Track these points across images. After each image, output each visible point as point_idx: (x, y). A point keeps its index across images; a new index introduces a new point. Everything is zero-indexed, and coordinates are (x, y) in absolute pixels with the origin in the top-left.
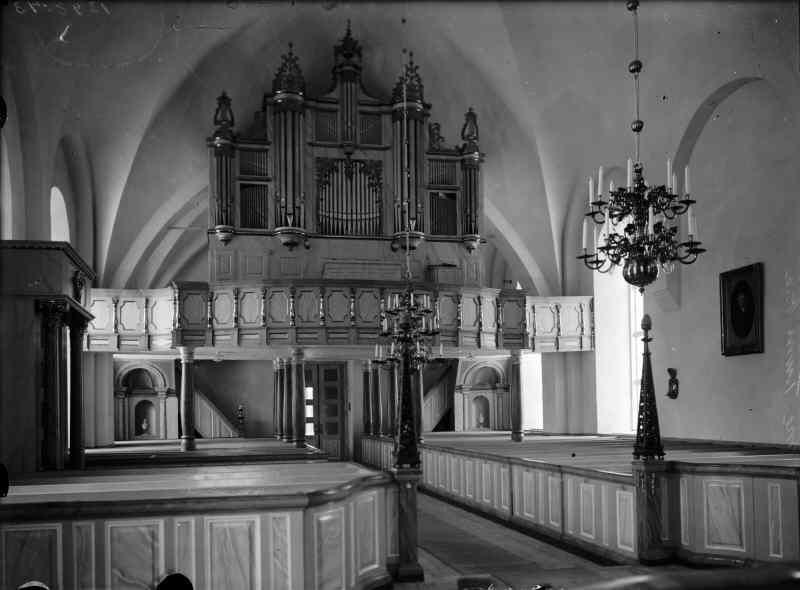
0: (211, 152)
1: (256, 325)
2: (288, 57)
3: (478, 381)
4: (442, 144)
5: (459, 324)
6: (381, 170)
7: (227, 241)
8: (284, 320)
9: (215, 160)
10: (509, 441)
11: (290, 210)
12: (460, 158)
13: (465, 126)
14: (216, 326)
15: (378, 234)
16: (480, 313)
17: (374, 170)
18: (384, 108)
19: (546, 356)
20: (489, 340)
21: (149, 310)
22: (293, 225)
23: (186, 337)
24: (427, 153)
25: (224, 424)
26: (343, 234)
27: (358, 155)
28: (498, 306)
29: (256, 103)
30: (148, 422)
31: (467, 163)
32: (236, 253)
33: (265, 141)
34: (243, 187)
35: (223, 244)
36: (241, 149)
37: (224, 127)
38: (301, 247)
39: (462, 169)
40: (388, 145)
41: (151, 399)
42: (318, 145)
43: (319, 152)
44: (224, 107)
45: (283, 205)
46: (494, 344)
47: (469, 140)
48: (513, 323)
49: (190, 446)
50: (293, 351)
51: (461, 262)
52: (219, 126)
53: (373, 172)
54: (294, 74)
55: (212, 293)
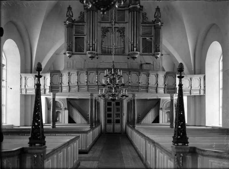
0: (65, 26)
1: (84, 85)
3: (167, 106)
4: (147, 20)
5: (149, 84)
6: (124, 31)
7: (70, 57)
8: (84, 83)
9: (66, 29)
10: (169, 128)
11: (91, 45)
12: (154, 25)
13: (156, 12)
14: (63, 85)
15: (123, 53)
16: (157, 80)
17: (122, 31)
18: (126, 8)
19: (188, 96)
20: (161, 91)
21: (45, 81)
22: (92, 50)
23: (53, 89)
24: (141, 24)
25: (83, 119)
26: (107, 53)
28: (165, 78)
31: (156, 26)
32: (73, 61)
33: (83, 22)
34: (76, 38)
35: (69, 57)
36: (76, 25)
37: (70, 18)
38: (95, 59)
39: (154, 29)
40: (127, 21)
41: (60, 111)
42: (102, 23)
43: (103, 25)
44: (70, 10)
45: (132, 43)
46: (163, 92)
47: (157, 18)
48: (171, 84)
49: (54, 126)
50: (90, 95)
51: (153, 63)
52: (68, 17)
53: (121, 31)
55: (62, 74)
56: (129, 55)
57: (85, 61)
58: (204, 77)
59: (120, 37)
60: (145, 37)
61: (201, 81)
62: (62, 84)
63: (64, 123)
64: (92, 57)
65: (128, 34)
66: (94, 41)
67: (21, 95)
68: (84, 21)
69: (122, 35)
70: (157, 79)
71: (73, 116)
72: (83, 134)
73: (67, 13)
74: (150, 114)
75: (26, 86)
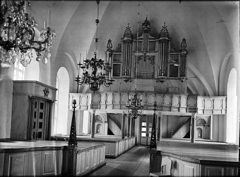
2: (127, 27)
3: (198, 123)
6: (155, 58)
11: (126, 71)
12: (180, 53)
26: (142, 77)
27: (148, 54)
29: (120, 41)
30: (100, 130)
36: (114, 55)
38: (129, 81)
41: (101, 123)
45: (161, 70)
53: (152, 59)
54: (129, 32)
56: (157, 79)
57: (121, 83)
58: (225, 98)
59: (151, 63)
60: (173, 64)
61: (223, 102)
62: (101, 102)
63: (104, 134)
64: (126, 81)
65: (158, 61)
66: (128, 68)
67: (68, 110)
68: (121, 51)
69: (153, 63)
70: (180, 100)
71: (111, 128)
72: (112, 143)
73: (108, 45)
74: (181, 129)
75: (81, 103)
